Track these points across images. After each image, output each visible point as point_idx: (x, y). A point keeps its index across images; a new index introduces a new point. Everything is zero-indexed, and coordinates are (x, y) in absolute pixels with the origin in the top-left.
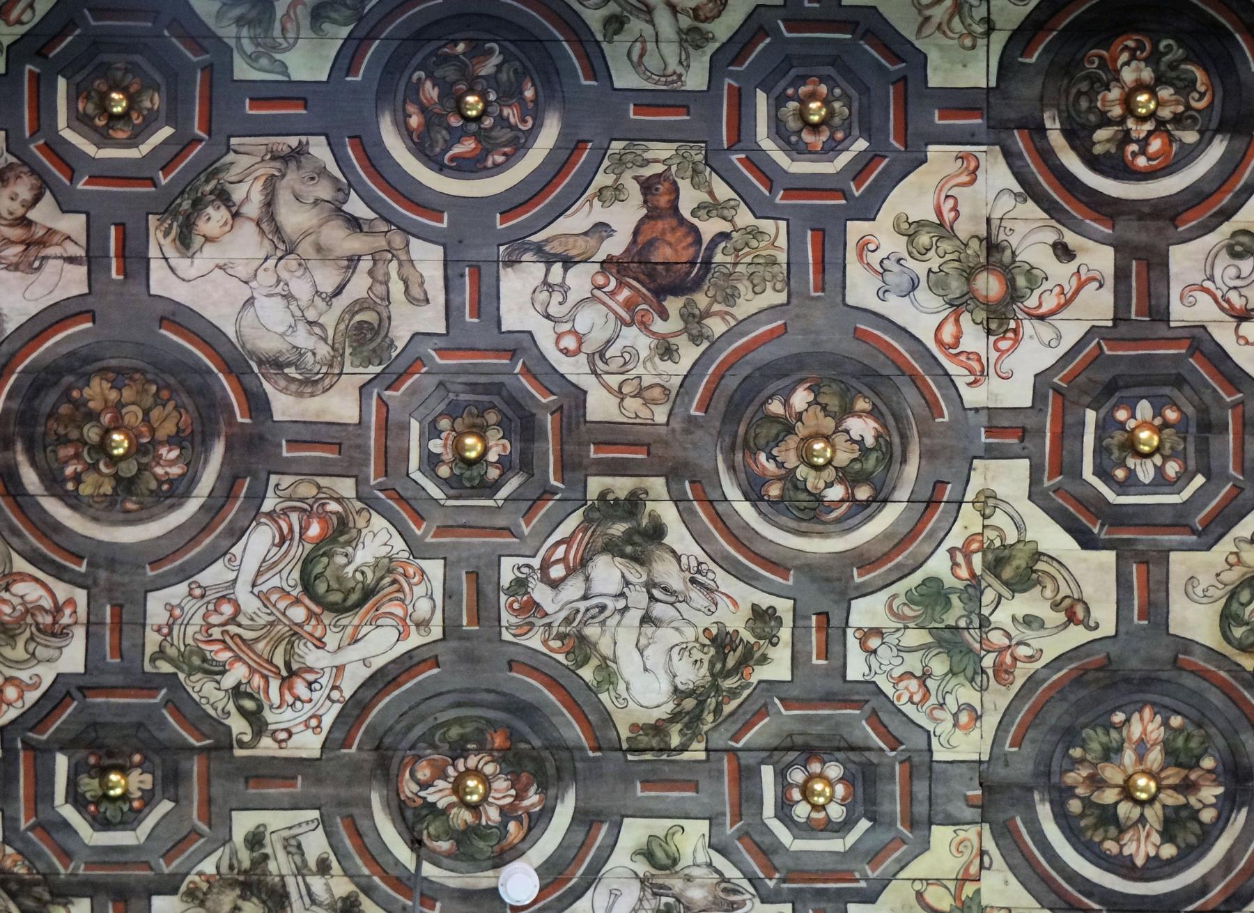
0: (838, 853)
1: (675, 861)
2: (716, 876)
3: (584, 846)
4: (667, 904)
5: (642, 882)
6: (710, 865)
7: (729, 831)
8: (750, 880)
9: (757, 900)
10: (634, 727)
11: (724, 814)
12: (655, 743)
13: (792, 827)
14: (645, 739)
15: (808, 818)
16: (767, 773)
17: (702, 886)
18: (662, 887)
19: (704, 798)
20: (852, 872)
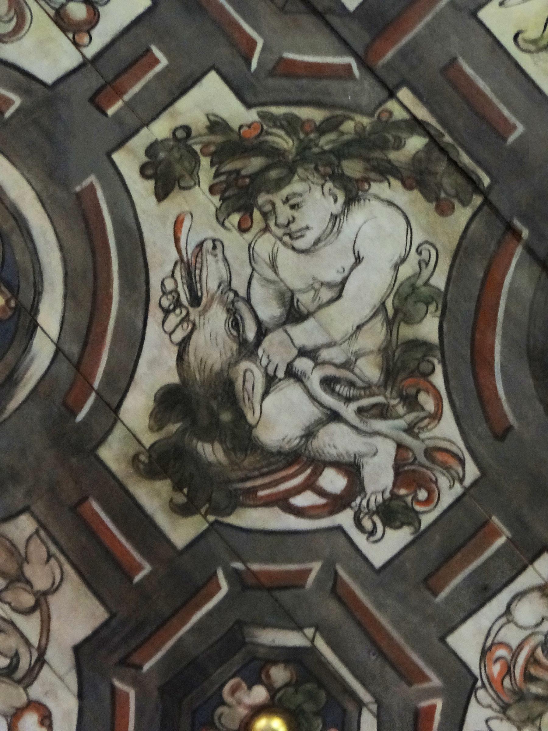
10: (443, 209)
14: (446, 182)
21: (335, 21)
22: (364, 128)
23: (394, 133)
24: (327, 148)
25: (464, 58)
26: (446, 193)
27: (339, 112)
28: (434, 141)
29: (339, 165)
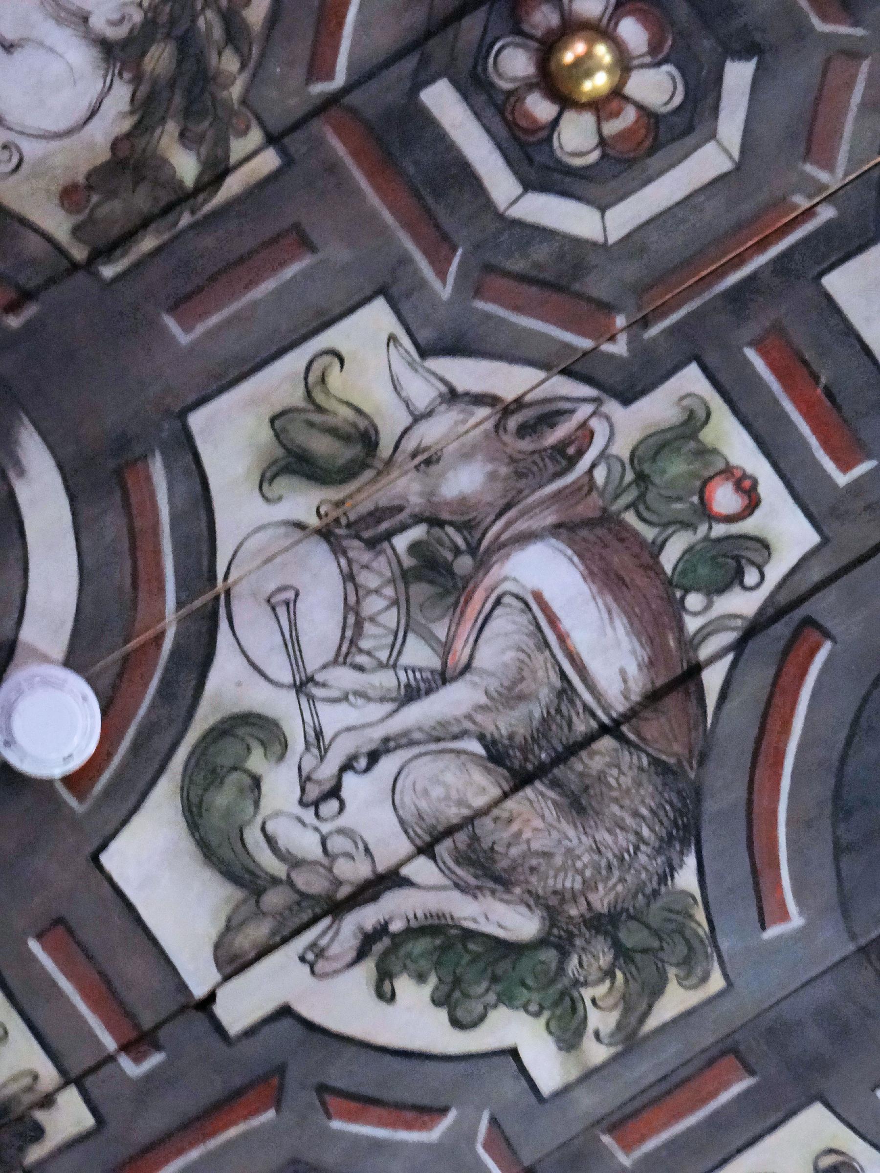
0: (721, 178)
1: (368, 439)
2: (483, 412)
3: (139, 540)
4: (415, 548)
5: (326, 534)
6: (452, 396)
7: (445, 292)
8: (566, 372)
9: (612, 407)
10: (70, 196)
11: (405, 260)
12: (142, 200)
13: (578, 187)
14: (115, 206)
15: (602, 142)
16: (443, 101)
17: (467, 455)
18: (378, 515)
19: (336, 252)
20: (781, 203)
21: (409, 64)
22: (226, 87)
23: (210, 134)
24: (201, 22)
25: (312, 267)
26: (98, 205)
27: (255, 51)
28: (184, 198)
29: (168, 36)
